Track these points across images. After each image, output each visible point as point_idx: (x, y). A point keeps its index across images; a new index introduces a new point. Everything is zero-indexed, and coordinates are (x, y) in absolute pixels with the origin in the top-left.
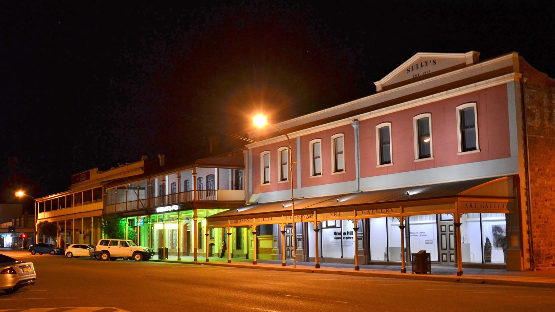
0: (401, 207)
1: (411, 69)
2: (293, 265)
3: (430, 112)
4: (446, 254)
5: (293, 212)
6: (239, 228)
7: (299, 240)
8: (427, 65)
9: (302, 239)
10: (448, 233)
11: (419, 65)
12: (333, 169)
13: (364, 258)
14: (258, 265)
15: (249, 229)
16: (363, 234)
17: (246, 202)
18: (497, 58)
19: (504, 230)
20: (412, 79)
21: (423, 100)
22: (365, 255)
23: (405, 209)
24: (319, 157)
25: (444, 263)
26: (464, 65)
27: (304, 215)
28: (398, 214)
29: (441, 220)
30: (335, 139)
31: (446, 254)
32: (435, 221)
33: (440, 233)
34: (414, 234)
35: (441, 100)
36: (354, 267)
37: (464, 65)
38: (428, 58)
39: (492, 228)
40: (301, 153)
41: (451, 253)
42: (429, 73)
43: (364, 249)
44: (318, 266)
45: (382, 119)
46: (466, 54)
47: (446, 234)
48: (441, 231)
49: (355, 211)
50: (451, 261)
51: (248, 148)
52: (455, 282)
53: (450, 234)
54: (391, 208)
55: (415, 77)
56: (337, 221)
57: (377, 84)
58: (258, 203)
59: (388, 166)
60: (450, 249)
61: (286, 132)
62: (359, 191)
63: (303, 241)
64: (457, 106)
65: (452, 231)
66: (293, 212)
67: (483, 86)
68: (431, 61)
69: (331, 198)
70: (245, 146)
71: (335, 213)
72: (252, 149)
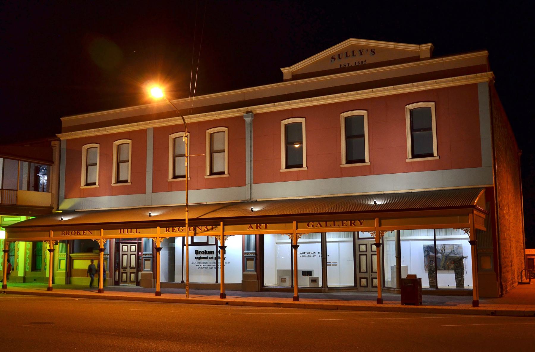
0: (295, 223)
1: (337, 57)
2: (185, 294)
3: (189, 131)
4: (367, 278)
5: (187, 222)
6: (39, 244)
7: (145, 260)
8: (361, 54)
9: (151, 259)
10: (369, 253)
11: (350, 53)
12: (207, 172)
13: (257, 282)
14: (54, 292)
15: (57, 244)
16: (256, 253)
17: (53, 208)
18: (480, 52)
19: (439, 250)
20: (340, 68)
21: (357, 94)
22: (258, 280)
23: (383, 221)
24: (127, 161)
25: (363, 289)
26: (417, 58)
27: (200, 227)
28: (51, 236)
29: (359, 238)
30: (211, 134)
31: (367, 278)
32: (352, 239)
33: (358, 253)
34: (310, 255)
35: (454, 86)
36: (376, 299)
37: (417, 58)
38: (364, 46)
39: (424, 248)
40: (154, 149)
41: (373, 277)
42: (364, 63)
43: (256, 272)
44: (223, 296)
45: (292, 113)
46: (421, 46)
47: (127, 255)
48: (360, 251)
49: (295, 223)
50: (373, 287)
51: (61, 139)
52: (489, 315)
53: (372, 255)
54: (359, 221)
55: (343, 66)
56: (436, 229)
57: (285, 70)
58: (75, 210)
59: (299, 171)
60: (372, 272)
61: (184, 113)
62: (250, 199)
63: (256, 259)
64: (207, 130)
65: (375, 251)
66: (187, 222)
67: (462, 82)
68: (367, 50)
69: (224, 206)
70: (56, 135)
71: (168, 229)
72: (68, 141)
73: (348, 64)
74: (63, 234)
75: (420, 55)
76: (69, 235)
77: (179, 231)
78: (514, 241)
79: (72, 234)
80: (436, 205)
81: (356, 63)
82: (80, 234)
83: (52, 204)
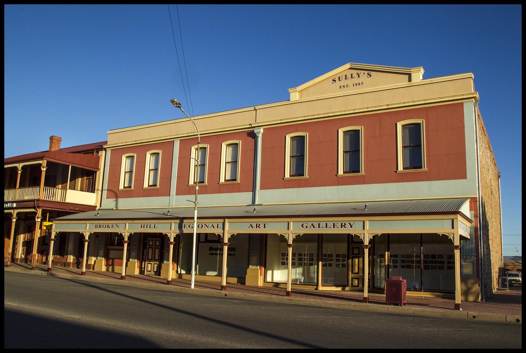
8: (359, 77)
28: (291, 229)
73: (347, 85)
74: (96, 227)
75: (361, 78)
76: (101, 228)
77: (303, 228)
78: (494, 251)
79: (189, 227)
80: (449, 210)
81: (354, 84)
82: (109, 228)
83: (96, 203)
